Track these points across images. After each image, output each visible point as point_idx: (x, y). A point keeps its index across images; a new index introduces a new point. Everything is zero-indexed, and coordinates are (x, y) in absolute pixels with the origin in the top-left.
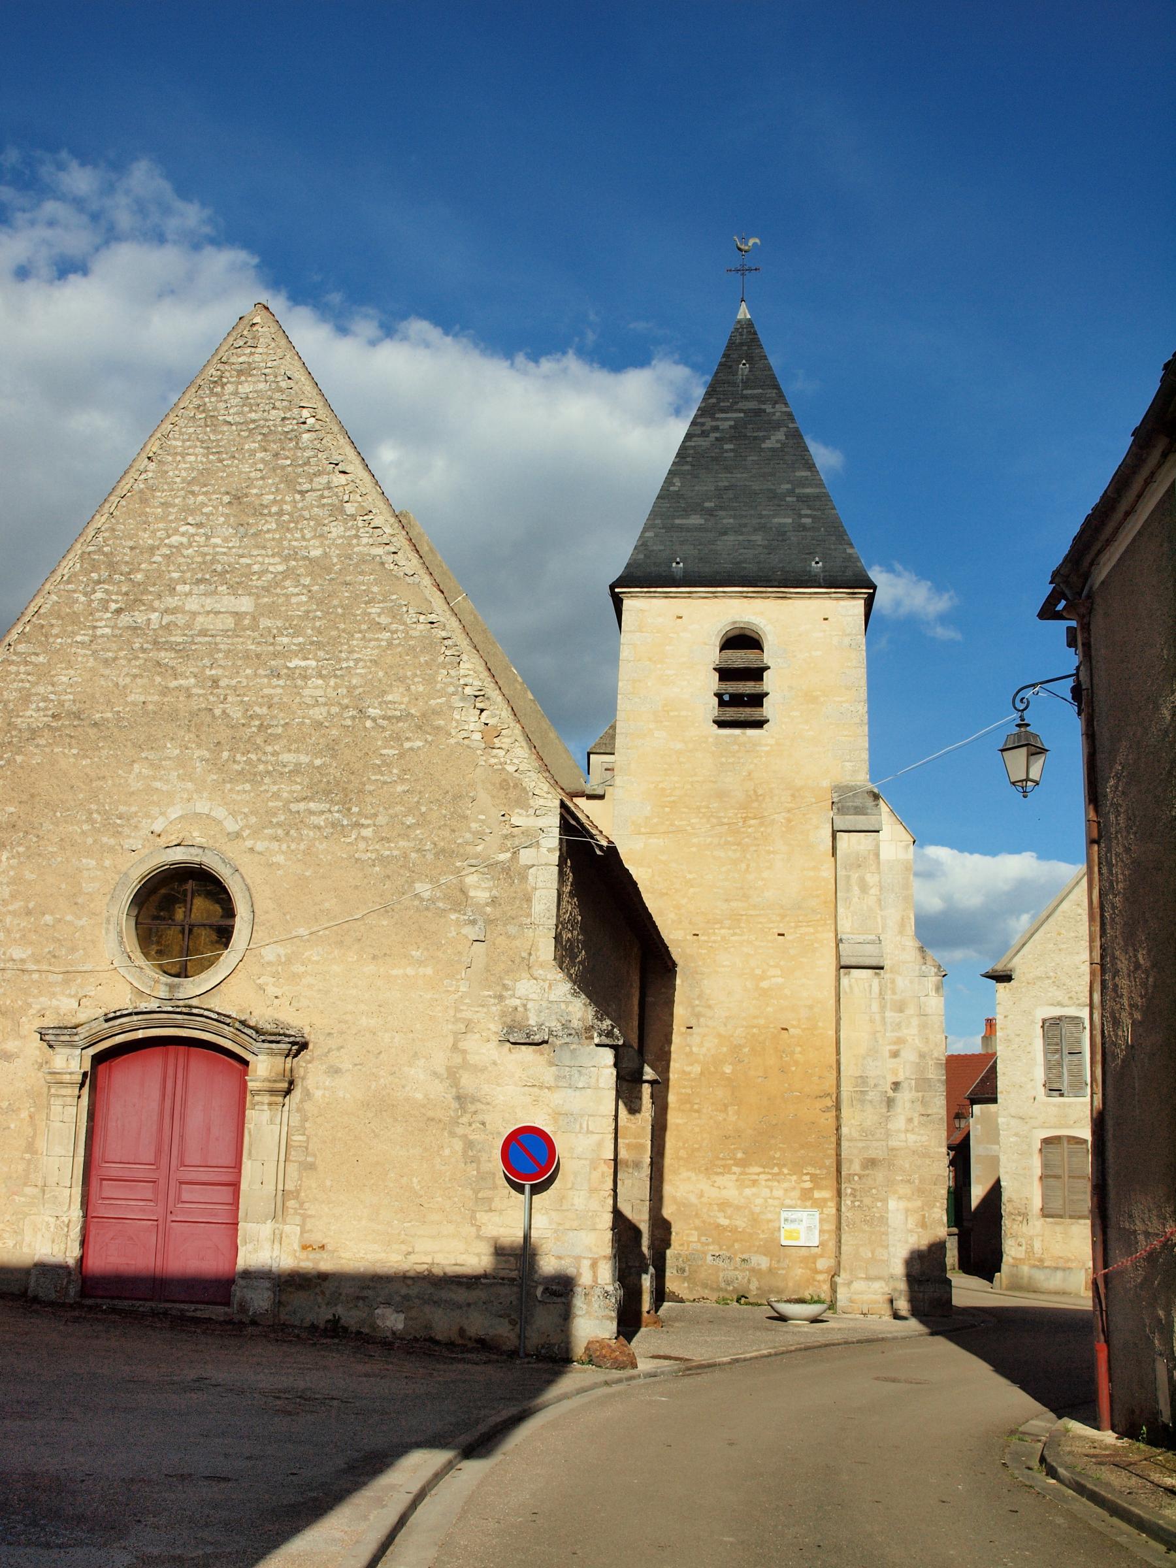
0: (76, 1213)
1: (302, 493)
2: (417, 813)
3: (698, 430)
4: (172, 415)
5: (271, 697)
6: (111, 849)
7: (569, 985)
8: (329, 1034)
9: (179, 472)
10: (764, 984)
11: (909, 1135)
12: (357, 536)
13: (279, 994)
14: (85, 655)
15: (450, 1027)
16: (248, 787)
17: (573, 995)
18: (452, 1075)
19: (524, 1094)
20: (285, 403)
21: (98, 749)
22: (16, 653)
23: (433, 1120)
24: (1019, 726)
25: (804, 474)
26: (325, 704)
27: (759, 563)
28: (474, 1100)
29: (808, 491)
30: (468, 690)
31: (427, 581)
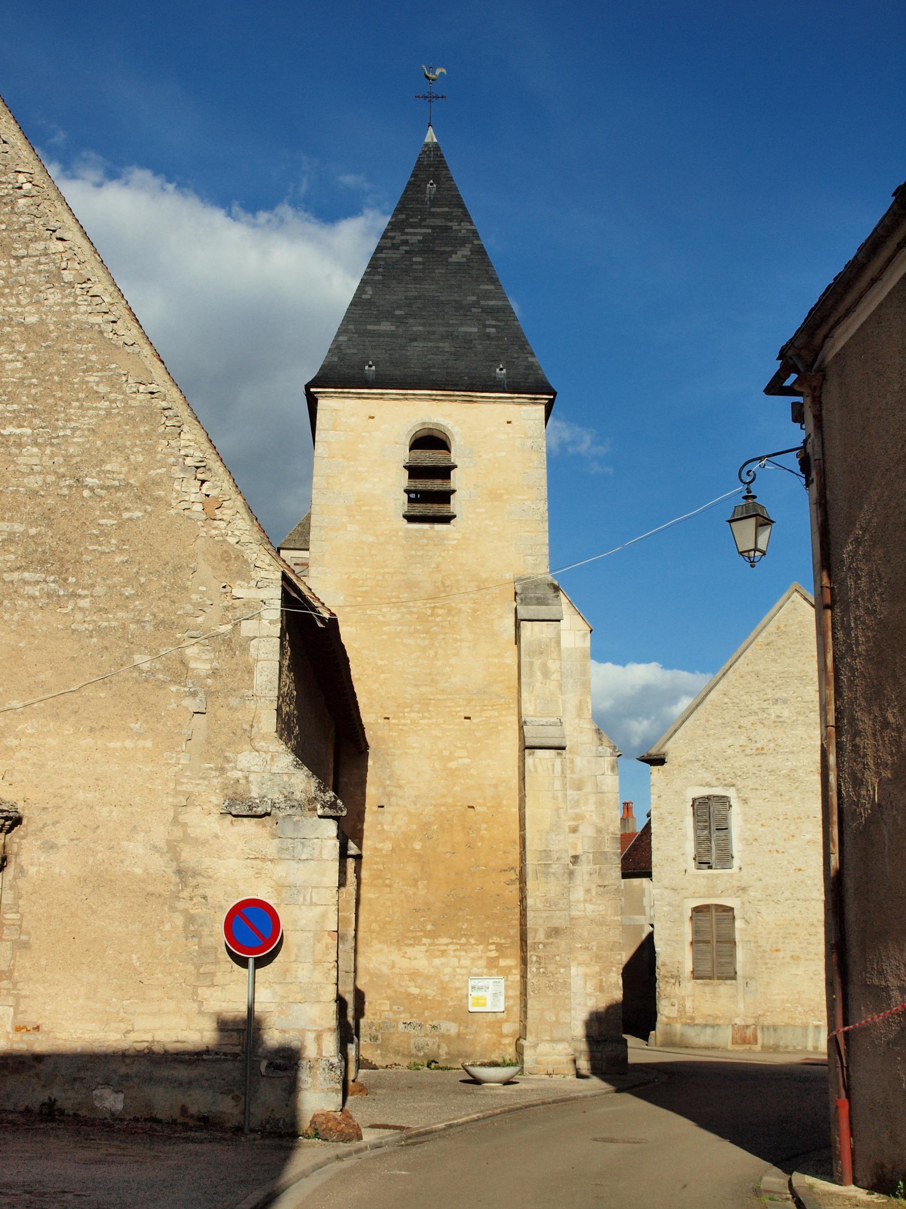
1: (18, 258)
2: (136, 584)
3: (388, 243)
7: (292, 757)
8: (44, 809)
10: (452, 765)
11: (587, 905)
12: (75, 304)
15: (170, 800)
17: (295, 766)
18: (172, 850)
19: (246, 867)
23: (152, 894)
24: (745, 498)
25: (487, 287)
26: (41, 473)
27: (447, 368)
28: (195, 874)
29: (492, 303)
30: (189, 461)
31: (147, 350)
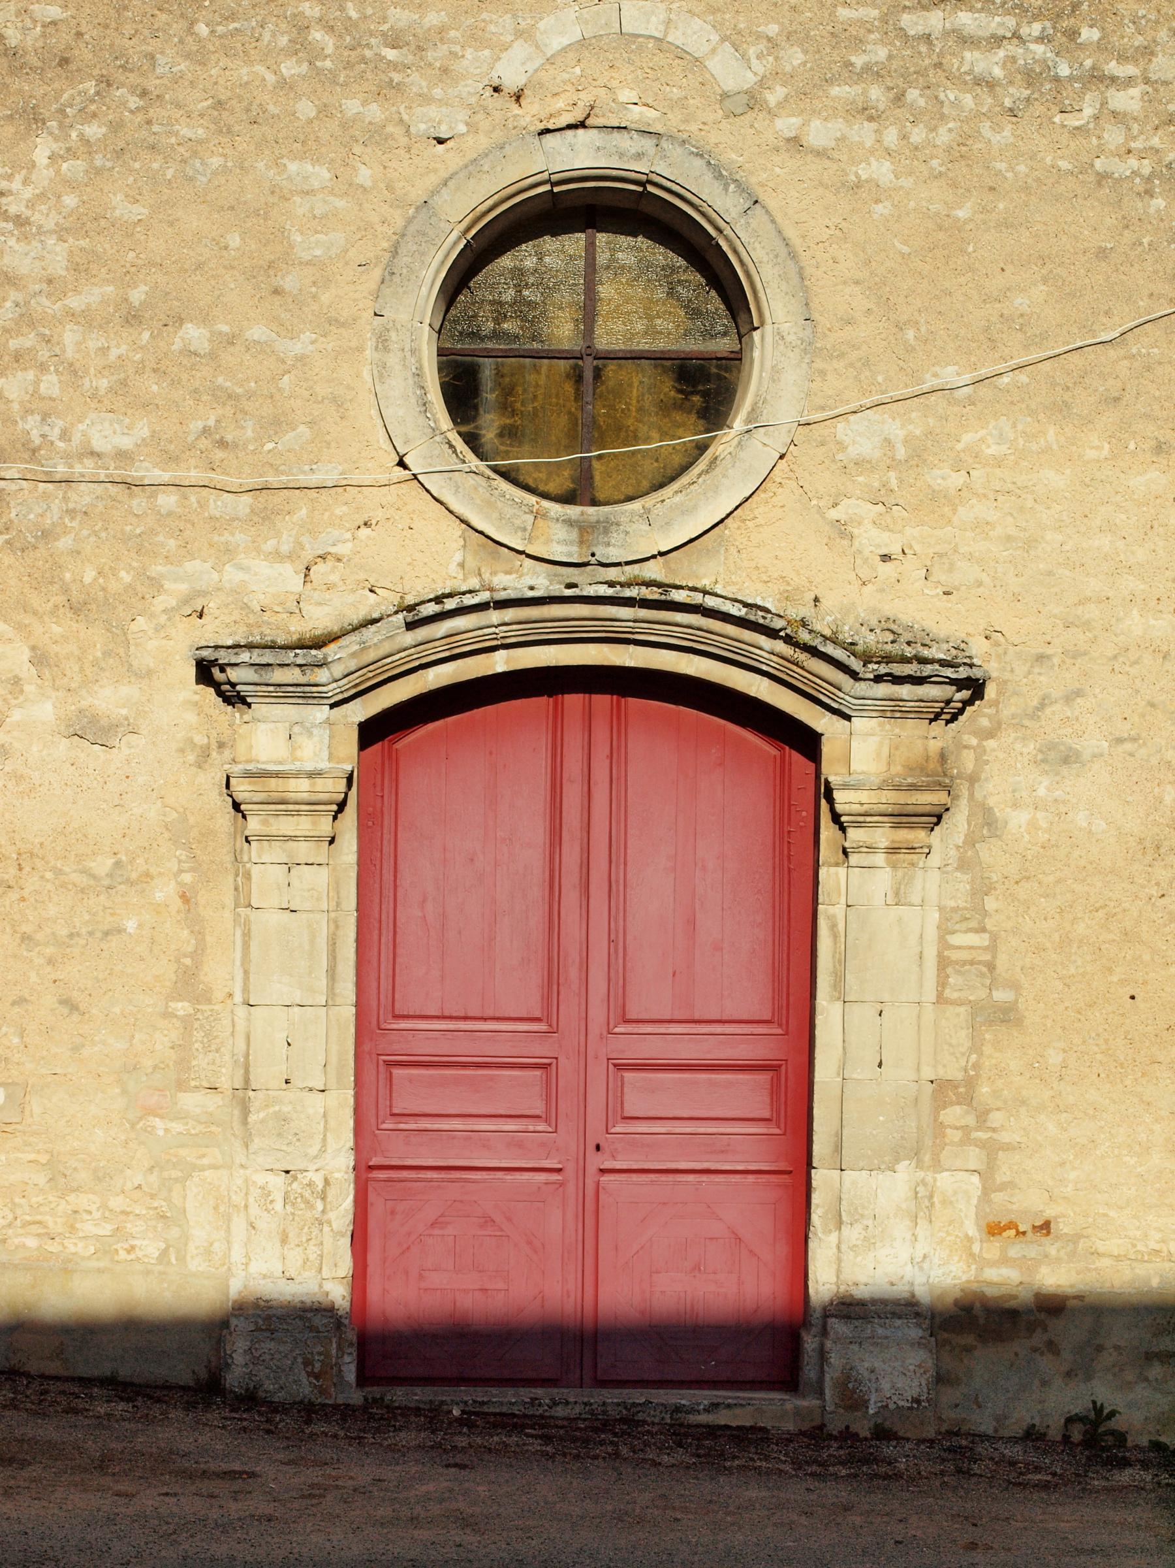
6: (376, 135)
8: (1041, 658)
13: (894, 549)
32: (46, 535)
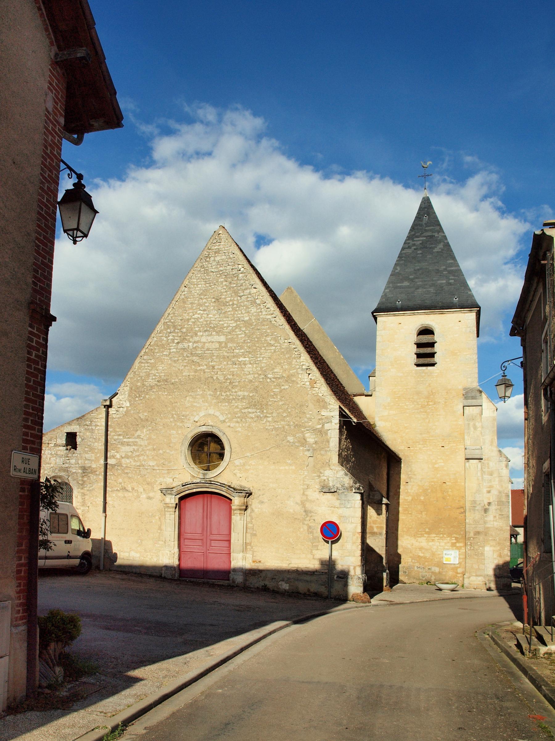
0: (176, 550)
1: (240, 297)
4: (192, 270)
5: (233, 372)
6: (181, 427)
9: (196, 291)
10: (436, 466)
12: (261, 312)
14: (167, 359)
16: (227, 404)
18: (303, 504)
20: (233, 263)
21: (174, 392)
22: (143, 359)
28: (311, 512)
30: (304, 367)
32: (145, 475)
